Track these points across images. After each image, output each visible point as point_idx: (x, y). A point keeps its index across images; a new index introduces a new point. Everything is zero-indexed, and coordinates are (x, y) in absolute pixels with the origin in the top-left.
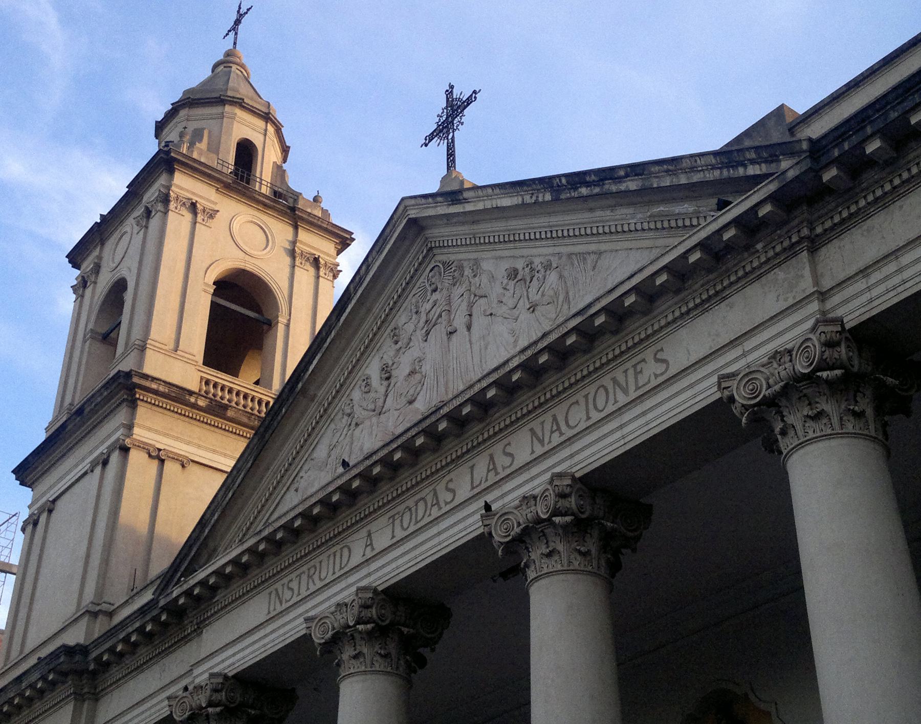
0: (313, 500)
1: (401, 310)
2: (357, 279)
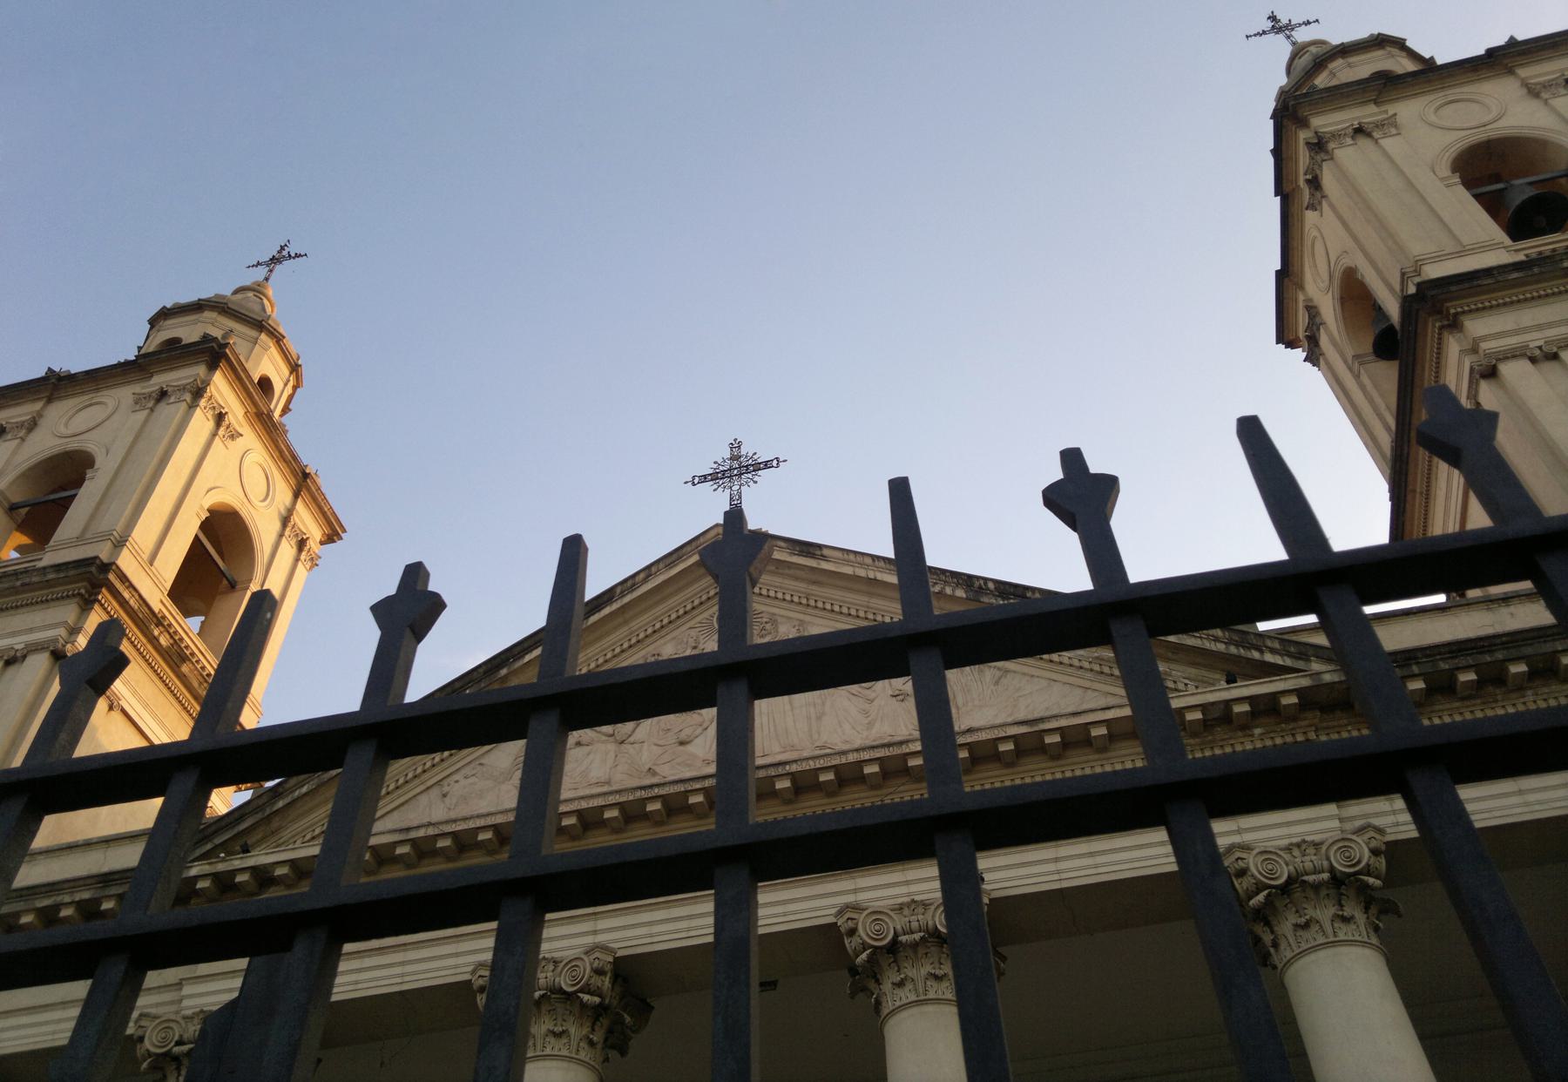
1: (668, 637)
2: (629, 583)
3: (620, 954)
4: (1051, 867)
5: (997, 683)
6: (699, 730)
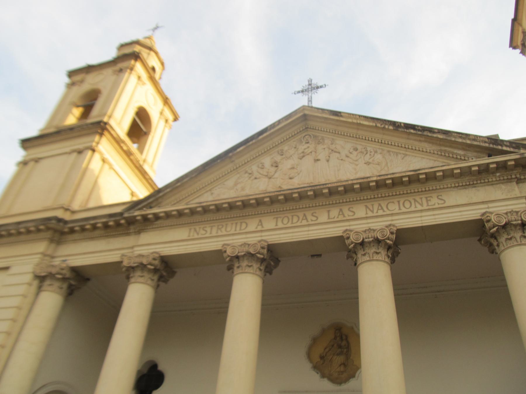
0: (389, 176)
3: (270, 243)
4: (419, 219)
5: (403, 159)
6: (297, 174)
